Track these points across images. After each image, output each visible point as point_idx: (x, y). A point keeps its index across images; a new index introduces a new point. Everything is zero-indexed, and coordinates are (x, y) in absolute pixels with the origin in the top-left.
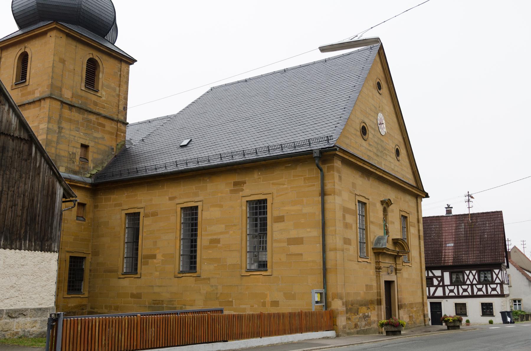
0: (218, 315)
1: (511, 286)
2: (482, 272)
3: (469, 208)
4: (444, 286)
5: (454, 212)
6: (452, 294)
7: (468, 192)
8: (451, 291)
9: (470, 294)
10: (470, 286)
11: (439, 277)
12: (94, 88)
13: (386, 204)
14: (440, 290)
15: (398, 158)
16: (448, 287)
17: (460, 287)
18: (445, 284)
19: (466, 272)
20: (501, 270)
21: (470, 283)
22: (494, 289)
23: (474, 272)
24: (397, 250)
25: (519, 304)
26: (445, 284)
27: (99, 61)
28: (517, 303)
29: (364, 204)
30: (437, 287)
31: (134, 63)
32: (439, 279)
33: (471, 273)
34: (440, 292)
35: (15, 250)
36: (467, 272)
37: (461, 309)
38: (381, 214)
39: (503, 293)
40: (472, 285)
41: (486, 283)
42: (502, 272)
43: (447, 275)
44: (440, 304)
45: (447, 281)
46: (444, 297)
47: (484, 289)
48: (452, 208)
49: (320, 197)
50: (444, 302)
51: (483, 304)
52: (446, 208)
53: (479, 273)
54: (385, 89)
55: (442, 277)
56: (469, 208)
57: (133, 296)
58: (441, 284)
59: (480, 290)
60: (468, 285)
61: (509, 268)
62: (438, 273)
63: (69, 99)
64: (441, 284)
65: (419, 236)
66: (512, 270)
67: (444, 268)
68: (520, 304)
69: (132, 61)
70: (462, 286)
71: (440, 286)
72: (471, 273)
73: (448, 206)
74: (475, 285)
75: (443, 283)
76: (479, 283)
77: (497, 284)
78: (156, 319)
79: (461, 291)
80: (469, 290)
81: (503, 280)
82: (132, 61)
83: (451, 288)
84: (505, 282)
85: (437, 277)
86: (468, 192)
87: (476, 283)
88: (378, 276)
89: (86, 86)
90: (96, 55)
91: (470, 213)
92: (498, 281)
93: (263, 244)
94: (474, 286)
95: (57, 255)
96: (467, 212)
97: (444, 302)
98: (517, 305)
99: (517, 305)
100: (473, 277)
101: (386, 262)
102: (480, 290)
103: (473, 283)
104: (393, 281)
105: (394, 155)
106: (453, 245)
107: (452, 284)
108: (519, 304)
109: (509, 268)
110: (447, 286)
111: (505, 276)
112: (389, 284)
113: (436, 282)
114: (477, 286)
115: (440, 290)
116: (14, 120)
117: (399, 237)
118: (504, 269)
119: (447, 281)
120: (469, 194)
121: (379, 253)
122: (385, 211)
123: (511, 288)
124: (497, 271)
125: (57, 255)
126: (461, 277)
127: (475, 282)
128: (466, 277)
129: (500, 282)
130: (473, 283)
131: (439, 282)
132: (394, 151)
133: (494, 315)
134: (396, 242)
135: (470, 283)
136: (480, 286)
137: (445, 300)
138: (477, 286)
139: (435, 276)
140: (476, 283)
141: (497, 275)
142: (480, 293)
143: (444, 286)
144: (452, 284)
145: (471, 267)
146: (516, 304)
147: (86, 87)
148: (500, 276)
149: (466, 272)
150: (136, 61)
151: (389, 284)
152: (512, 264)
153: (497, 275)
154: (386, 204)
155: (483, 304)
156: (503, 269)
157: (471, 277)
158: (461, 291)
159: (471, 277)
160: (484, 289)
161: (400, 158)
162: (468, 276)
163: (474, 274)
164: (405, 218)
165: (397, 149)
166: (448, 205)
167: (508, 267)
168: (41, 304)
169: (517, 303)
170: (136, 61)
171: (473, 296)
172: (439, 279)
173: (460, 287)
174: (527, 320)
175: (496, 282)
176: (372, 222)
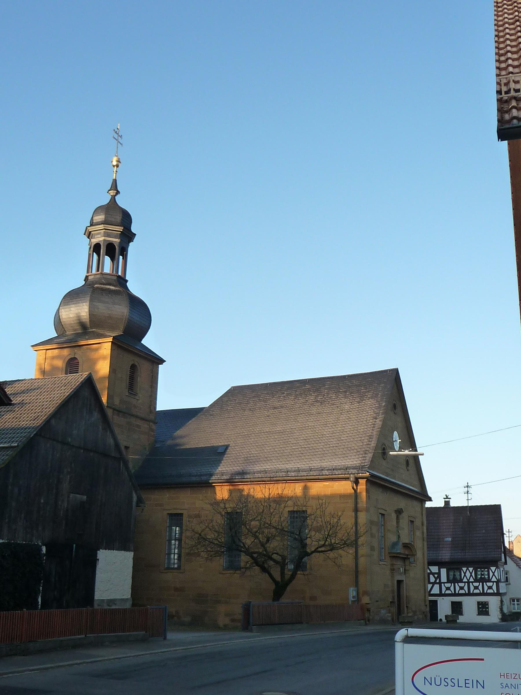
0: (138, 609)
1: (509, 584)
2: (479, 570)
3: (468, 500)
4: (440, 583)
5: (452, 504)
6: (448, 592)
7: (468, 483)
8: (448, 589)
9: (467, 592)
10: (466, 584)
11: (436, 573)
12: (132, 391)
13: (399, 512)
14: (437, 587)
15: (408, 468)
16: (445, 584)
17: (456, 584)
18: (442, 581)
19: (463, 568)
20: (497, 567)
21: (467, 581)
22: (490, 588)
23: (471, 569)
24: (407, 553)
25: (517, 604)
26: (442, 581)
27: (138, 366)
28: (516, 603)
29: (383, 515)
30: (434, 584)
31: (164, 364)
32: (436, 576)
33: (468, 571)
34: (436, 590)
35: (111, 550)
36: (464, 569)
37: (457, 608)
38: (395, 523)
39: (499, 592)
40: (468, 582)
41: (483, 580)
42: (499, 570)
43: (444, 571)
44: (436, 602)
45: (444, 578)
46: (441, 595)
47: (480, 588)
48: (450, 498)
49: (354, 513)
50: (440, 600)
51: (479, 603)
52: (444, 498)
53: (475, 570)
54: (399, 410)
55: (439, 574)
56: (468, 500)
57: (176, 589)
58: (438, 581)
59: (476, 588)
60: (465, 582)
61: (507, 564)
62: (434, 569)
63: (117, 405)
64: (438, 581)
65: (423, 538)
66: (511, 566)
67: (441, 564)
68: (519, 604)
69: (162, 361)
70: (459, 584)
71: (437, 583)
72: (468, 571)
73: (446, 496)
74: (472, 582)
75: (440, 580)
76: (476, 580)
77: (493, 582)
78: (17, 613)
79: (457, 588)
80: (466, 588)
81: (499, 578)
82: (162, 361)
83: (448, 585)
84: (502, 580)
85: (433, 574)
86: (468, 483)
87: (473, 581)
88: (393, 576)
89: (130, 392)
90: (137, 361)
91: (469, 505)
92: (494, 579)
94: (471, 584)
95: (132, 553)
96: (465, 505)
97: (440, 600)
98: (516, 604)
99: (516, 604)
100: (470, 574)
101: (399, 563)
102: (476, 588)
103: (470, 581)
104: (403, 581)
105: (404, 467)
106: (450, 539)
107: (448, 581)
108: (517, 604)
109: (507, 564)
110: (444, 583)
111: (501, 574)
112: (399, 582)
113: (432, 579)
114: (473, 583)
115: (437, 587)
116: (111, 441)
117: (407, 542)
118: (501, 565)
119: (444, 578)
120: (468, 486)
121: (394, 557)
122: (398, 518)
123: (509, 586)
124: (493, 569)
125: (132, 553)
126: (457, 574)
127: (472, 580)
128: (463, 574)
129: (496, 580)
130: (470, 581)
131: (436, 579)
132: (405, 463)
133: (490, 614)
134: (406, 546)
135: (467, 581)
136: (476, 584)
137: (441, 598)
138: (473, 583)
139: (431, 573)
140: (473, 581)
141: (494, 573)
142: (477, 591)
143: (440, 583)
144: (448, 581)
145: (467, 563)
146: (514, 604)
147: (129, 392)
148: (496, 574)
149: (463, 568)
150: (165, 361)
151: (399, 582)
152: (511, 558)
153: (494, 573)
154: (399, 512)
155: (479, 603)
156: (499, 566)
157: (468, 575)
158: (457, 588)
159: (468, 575)
160: (480, 588)
161: (409, 468)
162: (465, 573)
163: (471, 572)
164: (412, 522)
165: (407, 460)
166: (446, 495)
167: (506, 563)
168: (124, 595)
169: (516, 603)
170: (165, 361)
171: (469, 594)
172: (436, 576)
173: (456, 584)
174: (518, 619)
175: (492, 580)
176: (389, 530)
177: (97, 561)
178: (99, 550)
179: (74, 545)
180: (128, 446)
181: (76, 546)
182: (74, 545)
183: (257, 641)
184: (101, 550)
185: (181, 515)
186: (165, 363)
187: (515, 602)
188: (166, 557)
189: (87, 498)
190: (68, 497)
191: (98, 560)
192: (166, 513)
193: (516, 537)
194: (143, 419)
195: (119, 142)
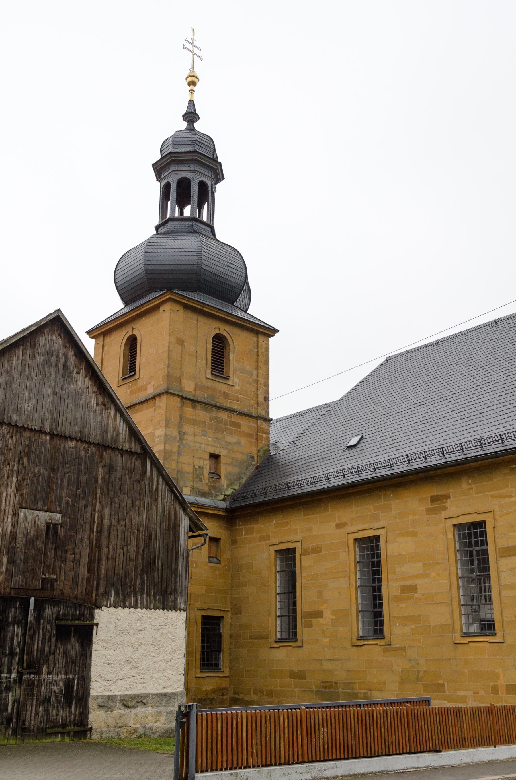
12: (223, 374)
27: (228, 337)
31: (276, 335)
57: (293, 675)
69: (271, 332)
82: (271, 332)
89: (213, 373)
90: (224, 329)
93: (485, 592)
147: (212, 374)
150: (277, 331)
170: (277, 331)
177: (95, 627)
178: (100, 608)
179: (32, 600)
180: (217, 452)
181: (36, 601)
182: (32, 600)
183: (11, 574)
184: (103, 608)
185: (294, 550)
186: (278, 333)
187: (475, 541)
188: (279, 622)
189: (62, 516)
190: (16, 514)
191: (97, 625)
192: (273, 549)
193: (166, 409)
194: (241, 414)
195: (195, 54)
